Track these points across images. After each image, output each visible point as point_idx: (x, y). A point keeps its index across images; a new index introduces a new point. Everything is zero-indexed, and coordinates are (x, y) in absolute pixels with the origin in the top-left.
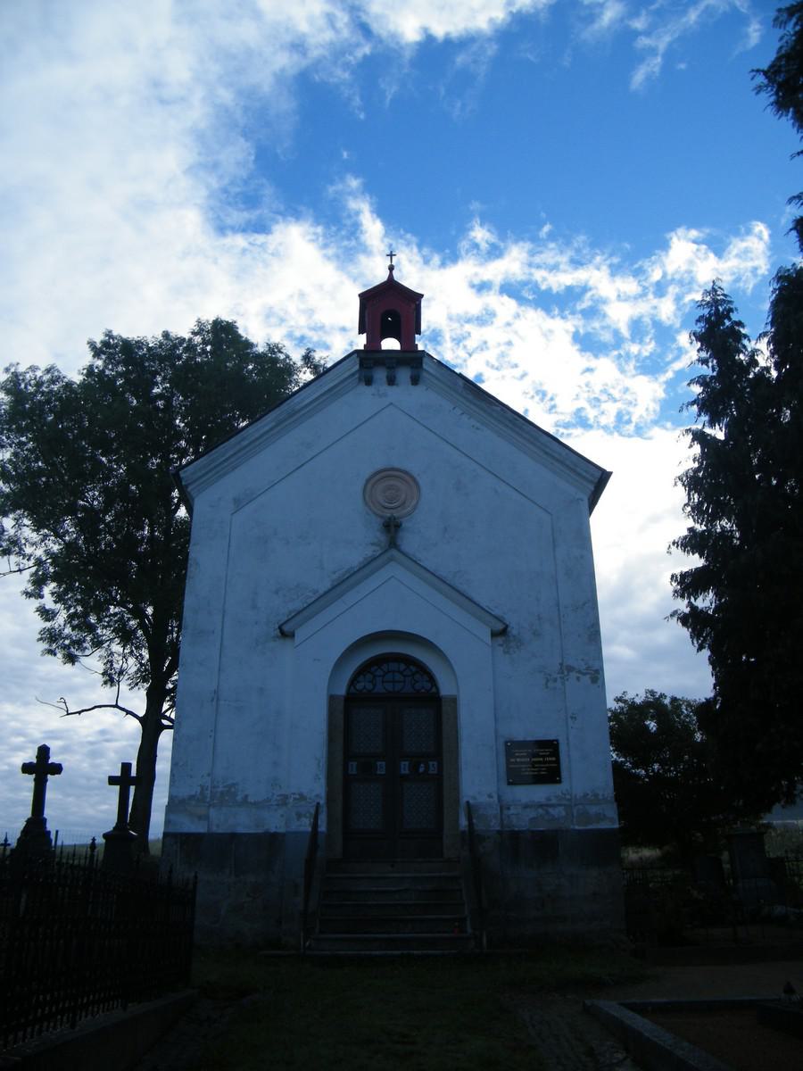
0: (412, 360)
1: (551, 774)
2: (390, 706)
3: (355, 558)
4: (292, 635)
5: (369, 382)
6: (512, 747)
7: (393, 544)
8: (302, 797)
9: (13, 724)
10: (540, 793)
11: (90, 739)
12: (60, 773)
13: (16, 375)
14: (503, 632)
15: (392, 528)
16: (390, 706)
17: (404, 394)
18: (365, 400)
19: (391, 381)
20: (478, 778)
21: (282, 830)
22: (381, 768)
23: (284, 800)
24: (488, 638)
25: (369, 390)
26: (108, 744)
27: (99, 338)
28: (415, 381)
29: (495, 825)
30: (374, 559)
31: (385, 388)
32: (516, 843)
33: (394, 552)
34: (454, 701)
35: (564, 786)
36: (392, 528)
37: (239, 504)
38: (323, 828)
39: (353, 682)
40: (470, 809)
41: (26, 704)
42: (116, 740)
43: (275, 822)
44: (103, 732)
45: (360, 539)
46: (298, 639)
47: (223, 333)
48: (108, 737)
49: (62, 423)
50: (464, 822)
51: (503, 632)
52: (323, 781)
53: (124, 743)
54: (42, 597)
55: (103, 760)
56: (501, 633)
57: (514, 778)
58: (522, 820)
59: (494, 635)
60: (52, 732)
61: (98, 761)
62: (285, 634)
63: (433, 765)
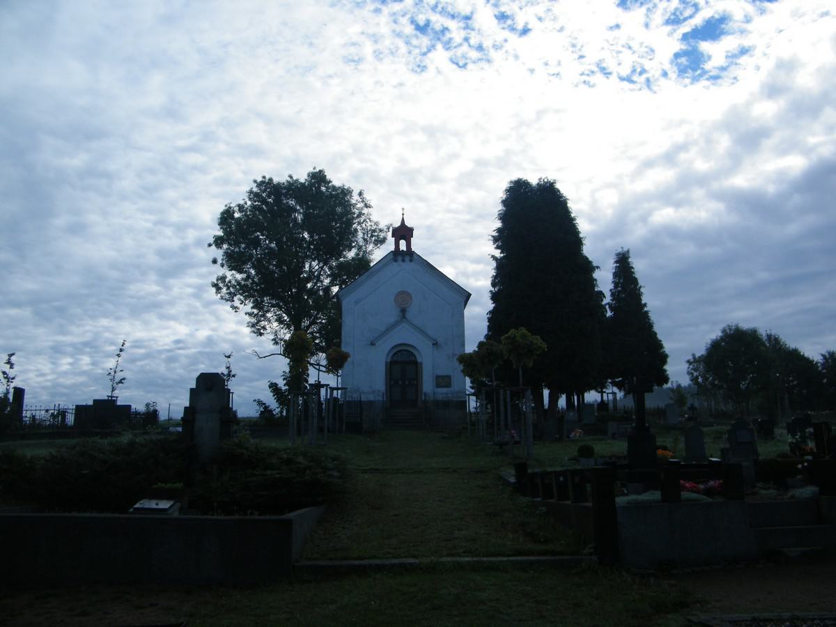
0: (410, 253)
1: (448, 385)
2: (403, 366)
3: (392, 320)
4: (375, 344)
5: (396, 261)
6: (438, 377)
7: (404, 317)
8: (379, 391)
9: (107, 335)
10: (444, 390)
11: (166, 347)
12: (202, 375)
13: (230, 208)
14: (436, 344)
15: (403, 311)
16: (403, 366)
17: (408, 265)
18: (395, 267)
19: (403, 261)
20: (428, 386)
21: (373, 400)
22: (400, 382)
23: (374, 392)
24: (431, 345)
25: (396, 264)
26: (181, 352)
27: (259, 179)
28: (411, 261)
29: (432, 399)
30: (398, 322)
31: (402, 263)
32: (437, 403)
33: (404, 320)
34: (421, 363)
35: (452, 388)
36: (403, 311)
37: (356, 302)
38: (385, 399)
39: (392, 357)
40: (425, 393)
41: (118, 318)
42: (189, 348)
43: (371, 397)
44: (178, 342)
45: (392, 315)
46: (377, 345)
47: (318, 178)
48: (181, 345)
49: (333, 314)
50: (423, 398)
51: (436, 344)
52: (384, 386)
53: (194, 350)
54: (233, 301)
55: (177, 365)
56: (435, 344)
57: (438, 385)
58: (440, 397)
59: (433, 344)
60: (136, 341)
61: (173, 365)
62: (372, 344)
63: (415, 382)
